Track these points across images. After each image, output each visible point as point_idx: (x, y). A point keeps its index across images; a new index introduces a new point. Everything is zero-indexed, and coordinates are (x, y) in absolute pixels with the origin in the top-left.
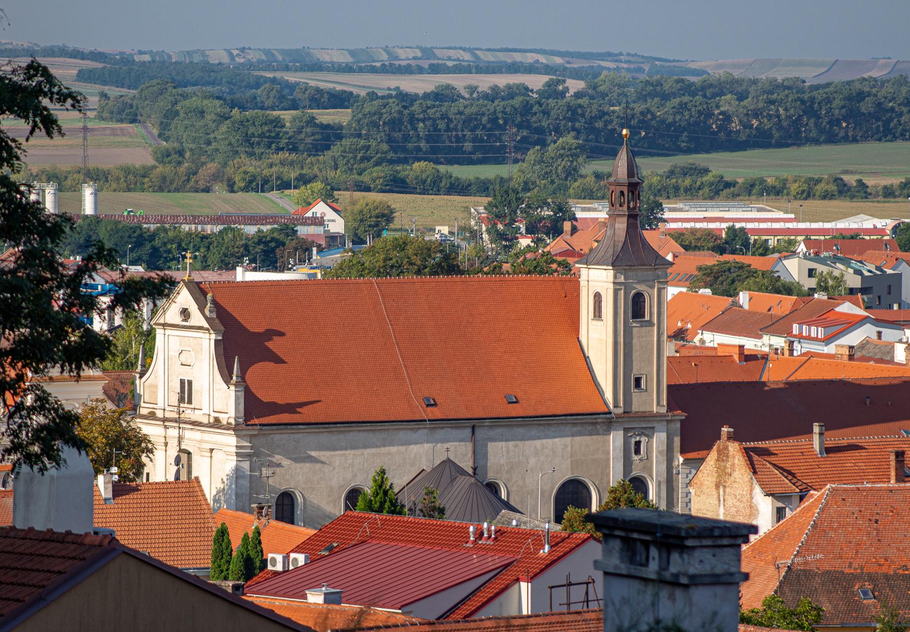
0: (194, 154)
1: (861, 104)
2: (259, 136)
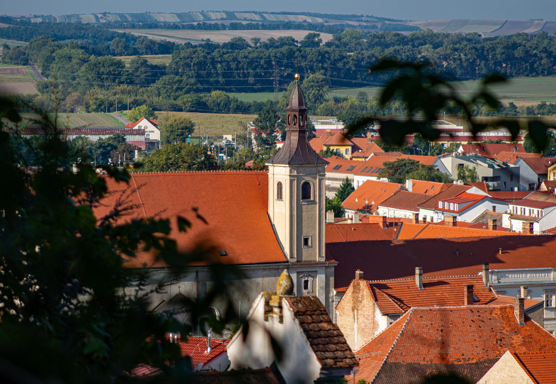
0: (64, 86)
1: (515, 51)
2: (107, 74)
